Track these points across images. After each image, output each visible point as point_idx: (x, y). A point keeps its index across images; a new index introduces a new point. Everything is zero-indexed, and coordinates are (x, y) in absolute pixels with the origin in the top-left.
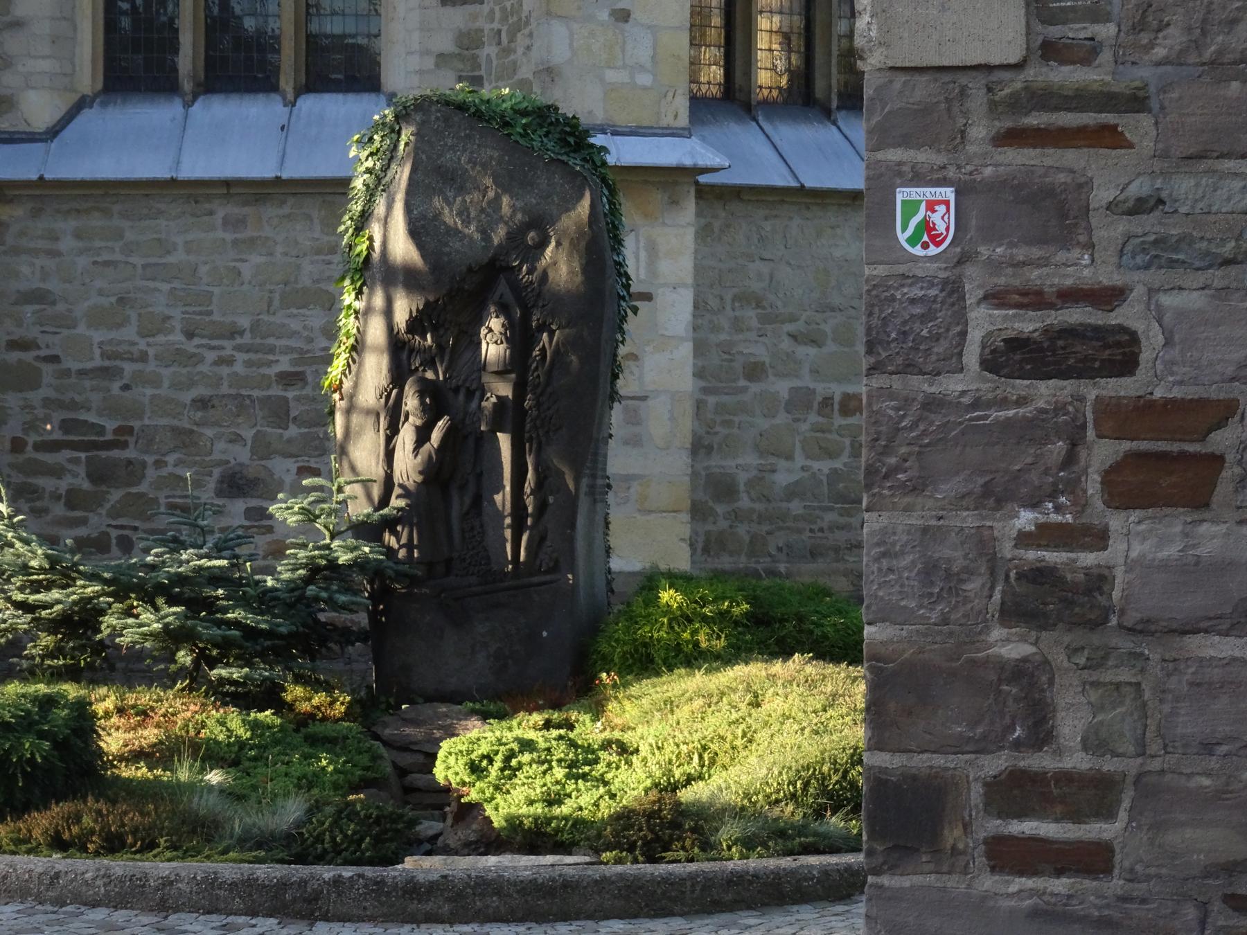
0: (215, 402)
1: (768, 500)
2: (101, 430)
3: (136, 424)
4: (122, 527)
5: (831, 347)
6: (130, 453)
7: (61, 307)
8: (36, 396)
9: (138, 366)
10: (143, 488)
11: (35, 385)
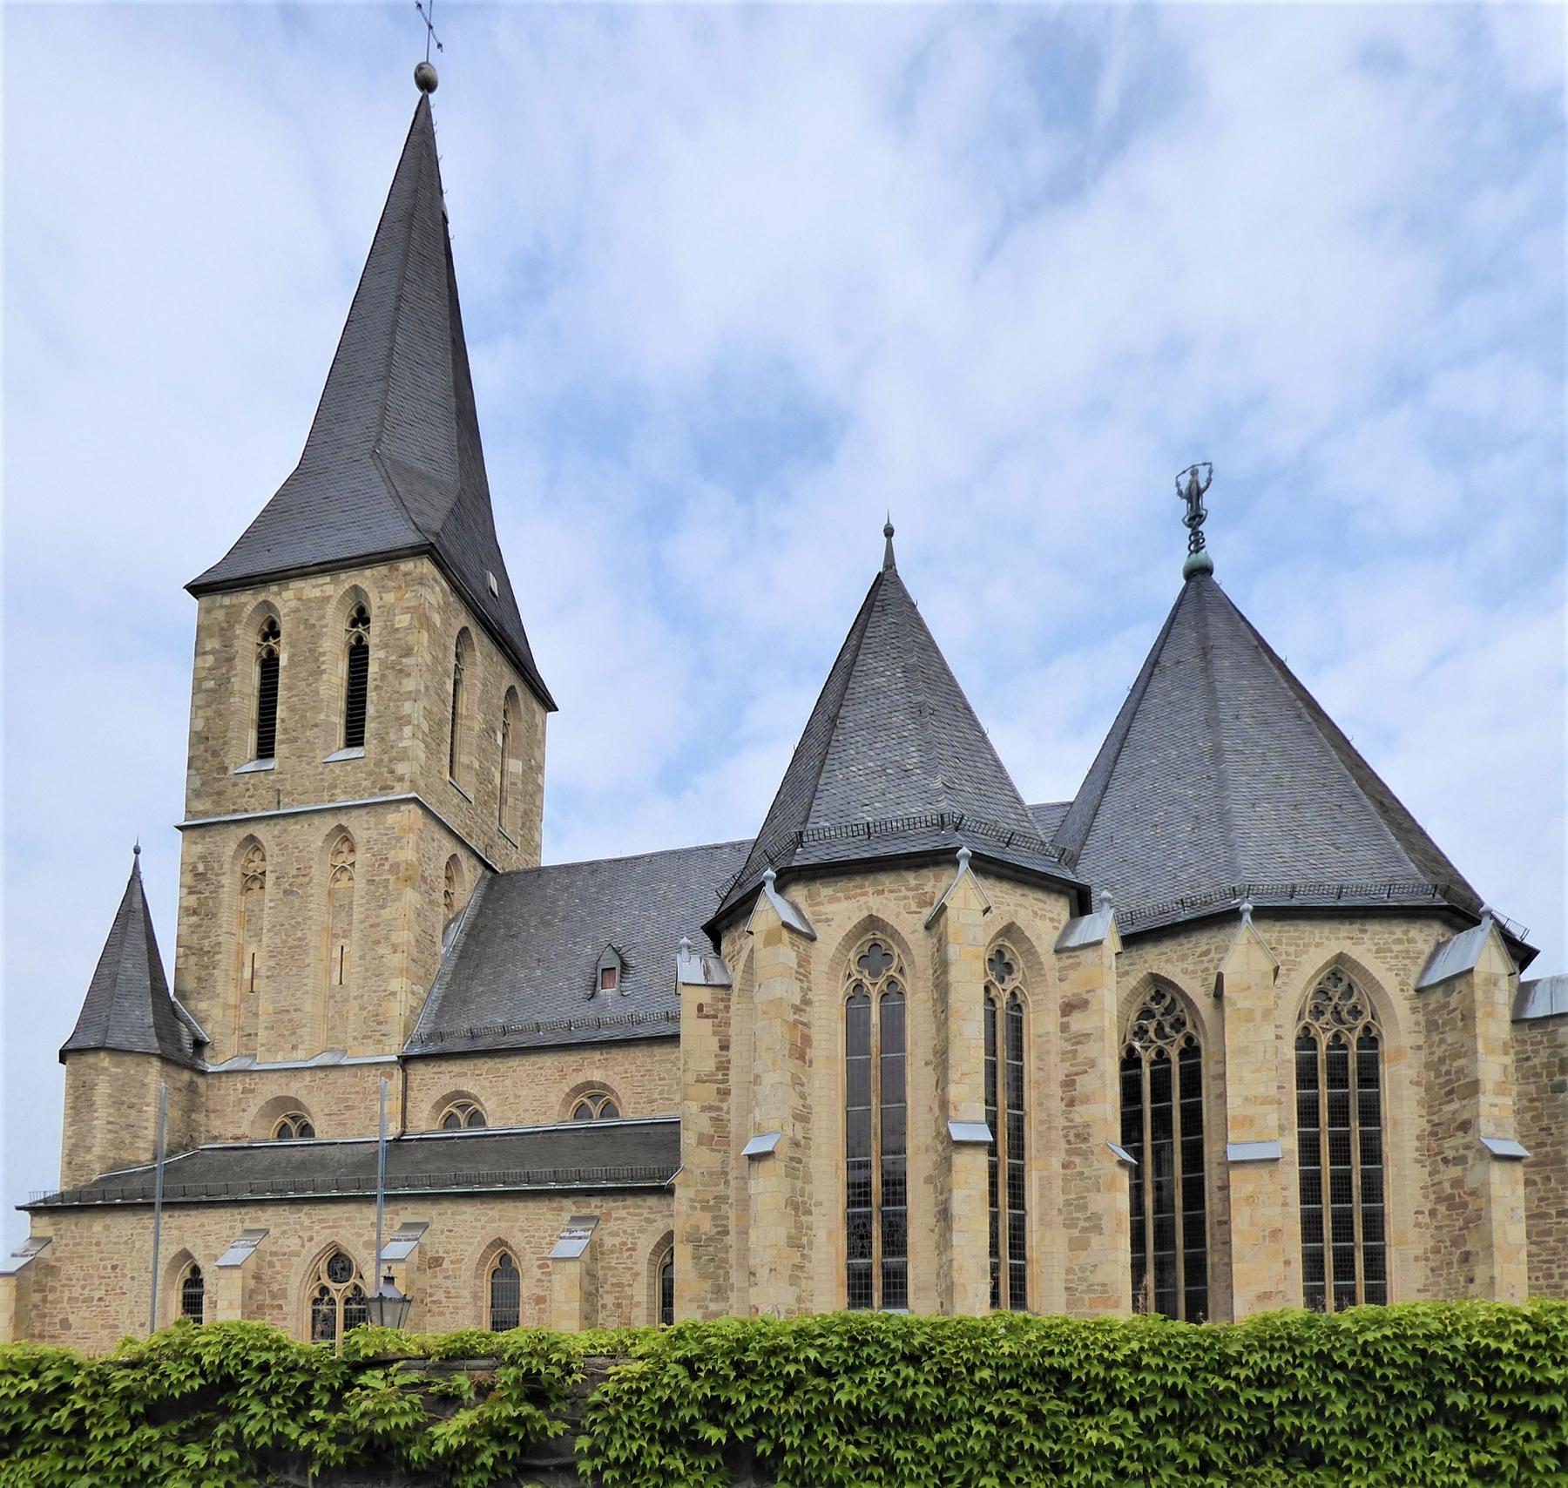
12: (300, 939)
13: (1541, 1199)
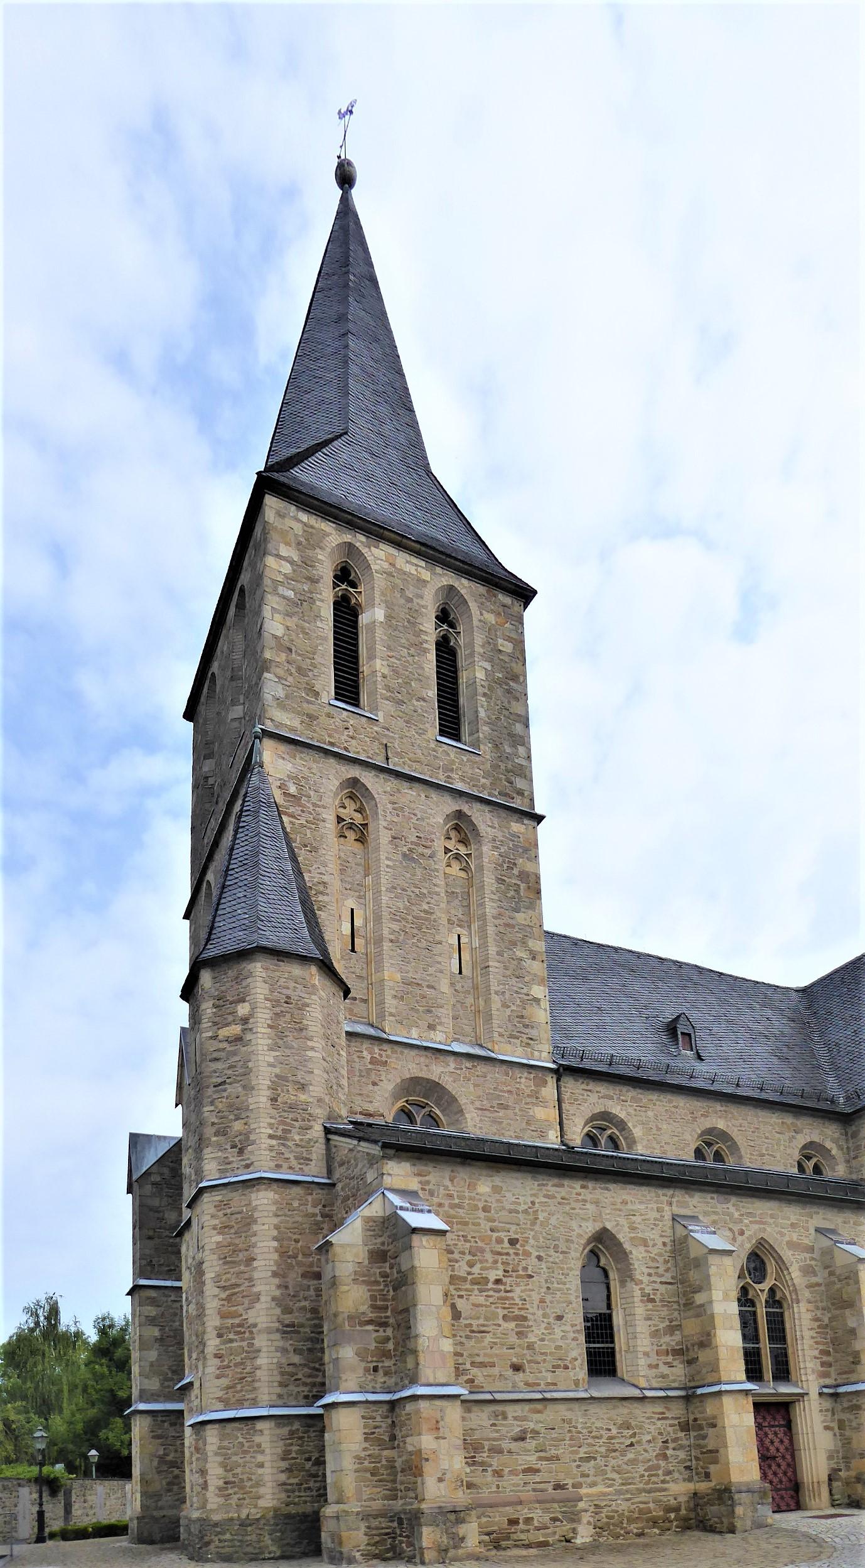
12: (425, 911)
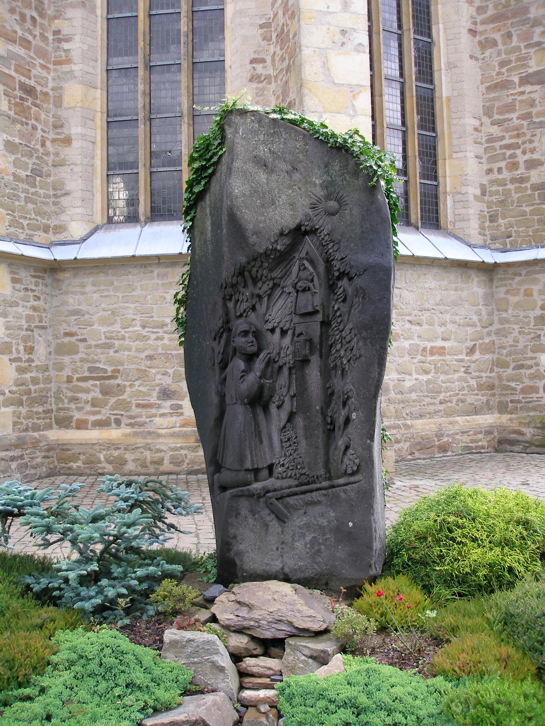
0: (156, 356)
1: (402, 393)
2: (106, 371)
3: (121, 368)
4: (117, 414)
5: (425, 326)
6: (119, 381)
7: (87, 317)
8: (77, 357)
9: (121, 342)
10: (125, 397)
11: (77, 352)
13: (502, 64)
